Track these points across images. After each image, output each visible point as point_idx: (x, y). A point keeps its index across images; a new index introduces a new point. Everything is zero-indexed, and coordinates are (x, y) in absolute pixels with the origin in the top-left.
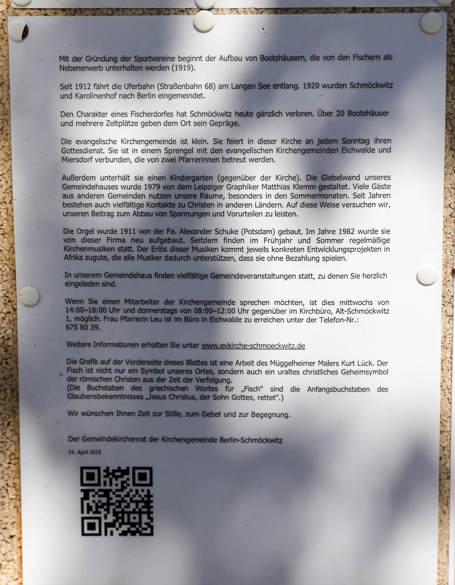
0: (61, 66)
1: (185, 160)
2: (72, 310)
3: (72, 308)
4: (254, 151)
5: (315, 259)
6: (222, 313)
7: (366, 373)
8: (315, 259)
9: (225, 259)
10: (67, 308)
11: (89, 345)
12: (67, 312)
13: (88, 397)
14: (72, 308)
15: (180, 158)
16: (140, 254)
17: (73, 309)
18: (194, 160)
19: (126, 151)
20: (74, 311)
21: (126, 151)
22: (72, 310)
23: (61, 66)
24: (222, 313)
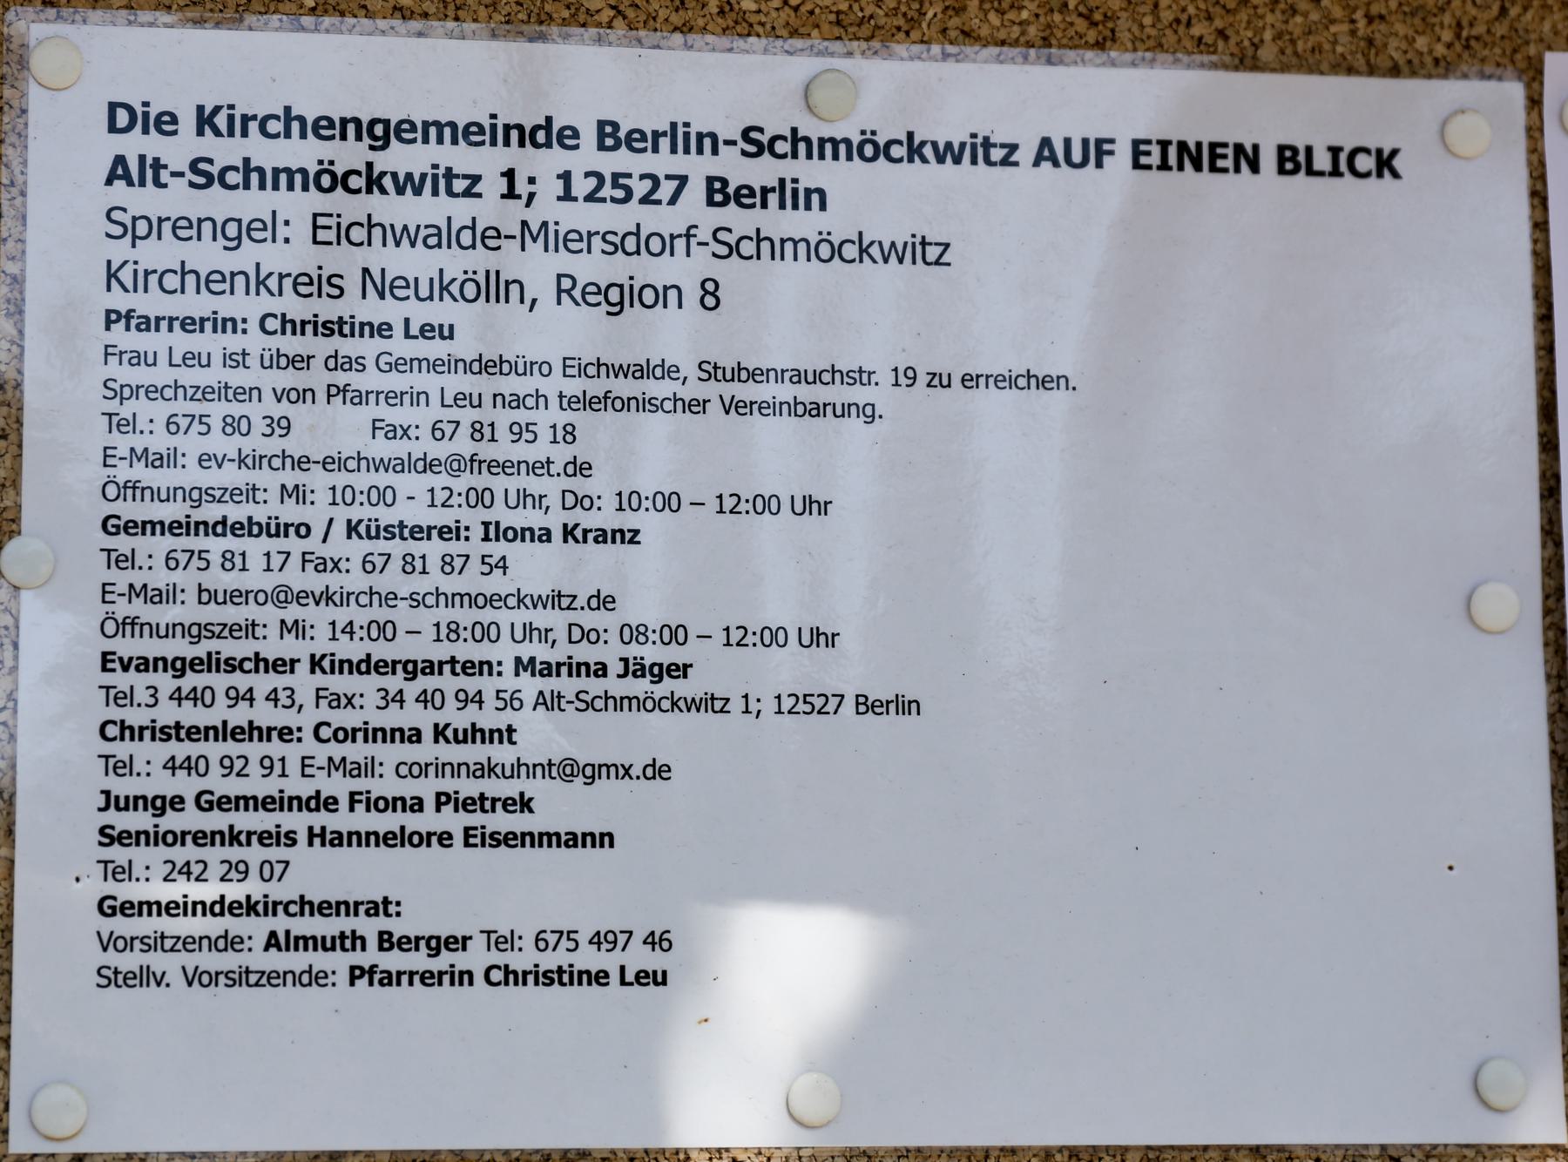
0: (366, 271)
1: (349, 395)
2: (352, 633)
3: (351, 623)
4: (648, 406)
5: (860, 410)
6: (738, 644)
7: (846, 379)
8: (860, 410)
9: (264, 981)
10: (333, 623)
11: (1248, 158)
12: (334, 639)
13: (271, 978)
14: (351, 623)
15: (334, 391)
16: (571, 518)
17: (356, 628)
18: (382, 397)
19: (240, 358)
20: (359, 633)
21: (240, 358)
22: (349, 629)
23: (366, 271)
24: (738, 644)
